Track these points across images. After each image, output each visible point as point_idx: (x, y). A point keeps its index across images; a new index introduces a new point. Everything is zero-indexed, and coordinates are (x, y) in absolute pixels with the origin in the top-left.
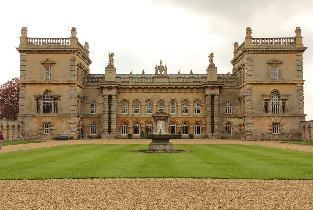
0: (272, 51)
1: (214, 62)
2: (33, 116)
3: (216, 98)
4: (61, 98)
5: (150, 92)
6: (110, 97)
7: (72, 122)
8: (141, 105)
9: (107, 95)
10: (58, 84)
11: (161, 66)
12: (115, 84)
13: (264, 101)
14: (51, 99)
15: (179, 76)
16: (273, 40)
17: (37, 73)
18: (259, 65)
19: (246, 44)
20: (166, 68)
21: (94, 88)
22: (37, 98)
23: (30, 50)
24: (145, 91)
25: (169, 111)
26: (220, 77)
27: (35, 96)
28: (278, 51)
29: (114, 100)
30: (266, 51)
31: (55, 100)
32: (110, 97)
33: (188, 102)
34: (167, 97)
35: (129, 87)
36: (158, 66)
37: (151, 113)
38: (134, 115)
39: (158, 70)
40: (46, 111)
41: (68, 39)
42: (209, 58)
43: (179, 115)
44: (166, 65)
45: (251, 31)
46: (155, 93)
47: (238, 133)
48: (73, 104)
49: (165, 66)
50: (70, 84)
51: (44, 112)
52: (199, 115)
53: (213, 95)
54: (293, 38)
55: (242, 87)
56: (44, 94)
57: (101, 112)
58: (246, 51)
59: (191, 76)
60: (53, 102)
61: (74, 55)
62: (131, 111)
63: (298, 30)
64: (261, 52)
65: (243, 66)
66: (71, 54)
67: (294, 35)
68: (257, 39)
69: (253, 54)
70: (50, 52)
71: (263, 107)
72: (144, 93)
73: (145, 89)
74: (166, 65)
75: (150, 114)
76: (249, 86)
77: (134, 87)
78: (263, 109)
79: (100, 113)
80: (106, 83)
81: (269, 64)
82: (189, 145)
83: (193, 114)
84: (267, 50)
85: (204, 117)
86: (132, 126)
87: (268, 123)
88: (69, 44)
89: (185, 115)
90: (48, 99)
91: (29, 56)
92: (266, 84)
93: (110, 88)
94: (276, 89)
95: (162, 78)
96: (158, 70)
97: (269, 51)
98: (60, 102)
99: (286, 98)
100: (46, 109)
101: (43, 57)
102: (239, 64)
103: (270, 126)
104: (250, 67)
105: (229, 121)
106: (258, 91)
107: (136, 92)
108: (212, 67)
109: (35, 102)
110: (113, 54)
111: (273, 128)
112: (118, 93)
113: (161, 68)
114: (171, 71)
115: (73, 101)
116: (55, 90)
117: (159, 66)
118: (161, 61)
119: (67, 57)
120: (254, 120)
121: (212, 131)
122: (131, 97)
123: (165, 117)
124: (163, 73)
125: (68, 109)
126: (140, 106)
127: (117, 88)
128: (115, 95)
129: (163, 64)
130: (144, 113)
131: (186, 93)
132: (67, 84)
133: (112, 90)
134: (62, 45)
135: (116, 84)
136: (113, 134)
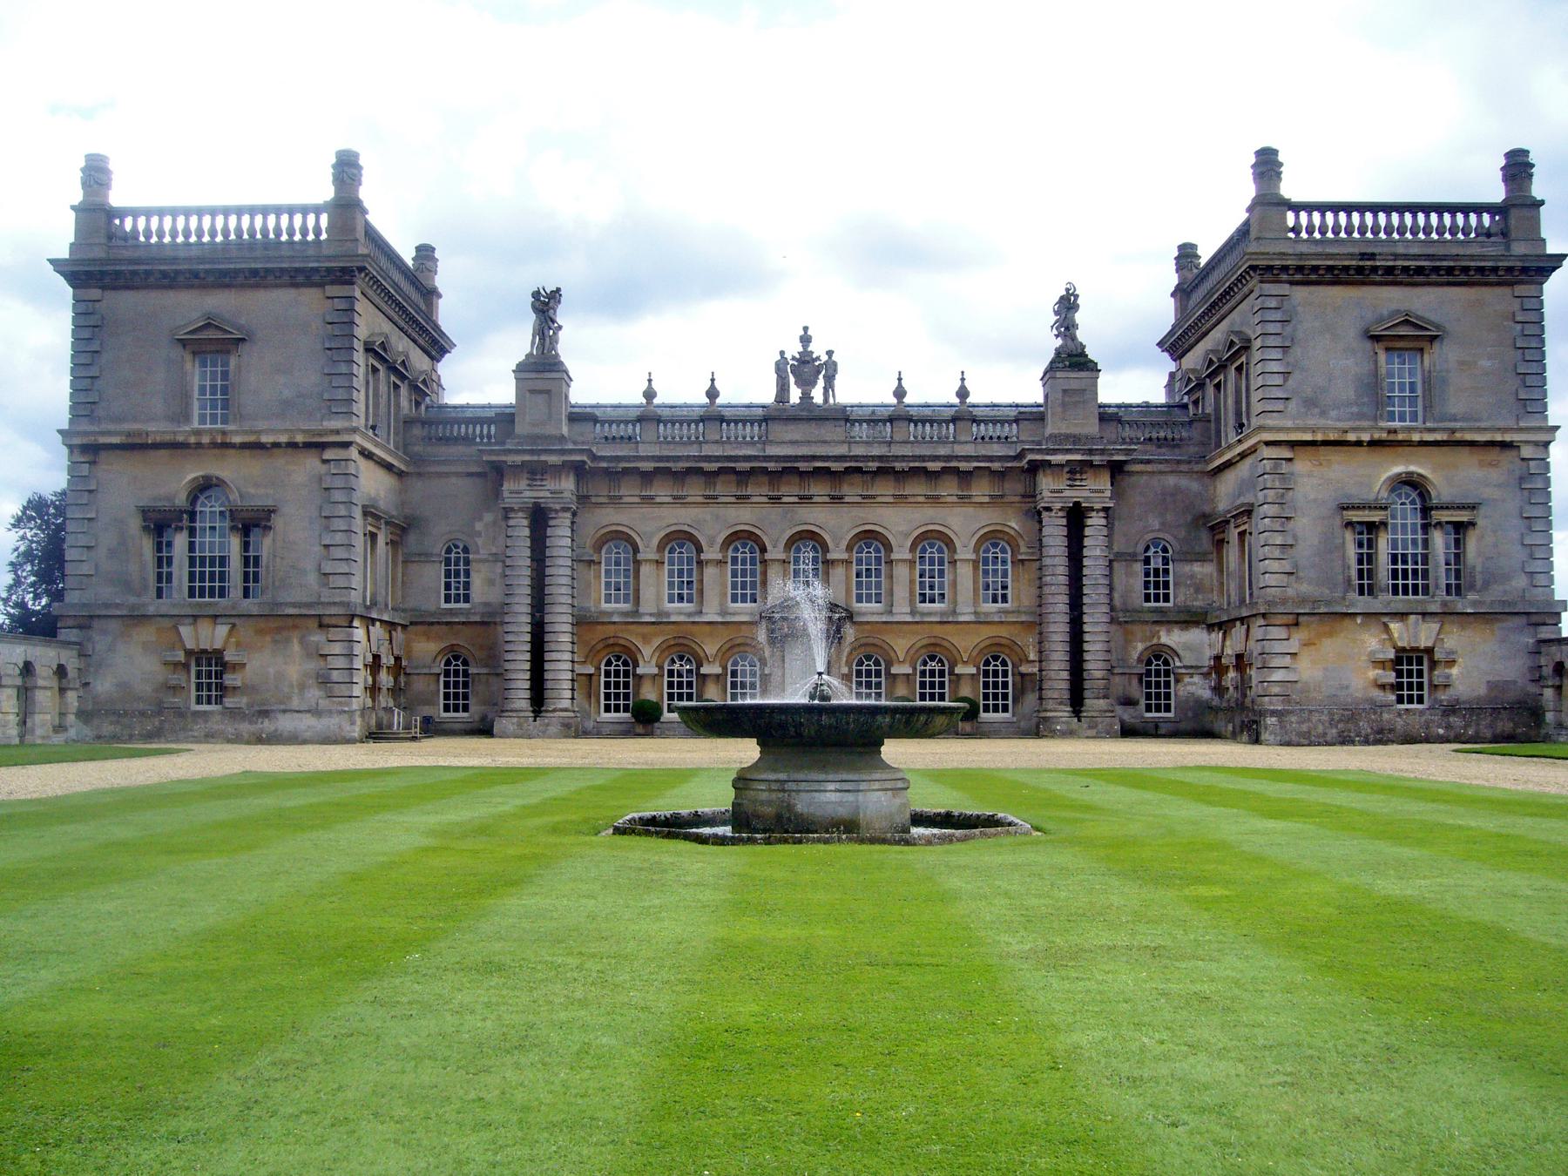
2: (137, 618)
3: (1095, 522)
4: (277, 522)
6: (539, 518)
9: (521, 510)
12: (563, 452)
20: (831, 370)
21: (457, 474)
22: (159, 524)
25: (848, 591)
27: (145, 512)
28: (1420, 271)
29: (560, 536)
32: (539, 518)
33: (950, 543)
36: (788, 356)
38: (668, 614)
39: (792, 379)
41: (317, 210)
42: (1056, 313)
43: (902, 612)
44: (830, 353)
46: (775, 500)
49: (824, 358)
50: (322, 446)
52: (1006, 612)
55: (1229, 465)
63: (1517, 167)
66: (333, 290)
67: (1495, 192)
68: (1309, 208)
69: (1292, 283)
74: (830, 353)
76: (1268, 452)
78: (1349, 580)
81: (1376, 339)
88: (324, 236)
89: (930, 614)
91: (124, 302)
93: (536, 472)
94: (1412, 468)
97: (1374, 269)
103: (1382, 664)
104: (1276, 354)
106: (1319, 483)
109: (147, 545)
110: (556, 295)
112: (583, 499)
113: (806, 367)
114: (859, 388)
116: (245, 479)
118: (806, 329)
120: (1298, 636)
121: (1076, 700)
125: (312, 579)
127: (579, 470)
129: (818, 349)
131: (934, 500)
133: (550, 484)
135: (571, 452)
136: (554, 710)
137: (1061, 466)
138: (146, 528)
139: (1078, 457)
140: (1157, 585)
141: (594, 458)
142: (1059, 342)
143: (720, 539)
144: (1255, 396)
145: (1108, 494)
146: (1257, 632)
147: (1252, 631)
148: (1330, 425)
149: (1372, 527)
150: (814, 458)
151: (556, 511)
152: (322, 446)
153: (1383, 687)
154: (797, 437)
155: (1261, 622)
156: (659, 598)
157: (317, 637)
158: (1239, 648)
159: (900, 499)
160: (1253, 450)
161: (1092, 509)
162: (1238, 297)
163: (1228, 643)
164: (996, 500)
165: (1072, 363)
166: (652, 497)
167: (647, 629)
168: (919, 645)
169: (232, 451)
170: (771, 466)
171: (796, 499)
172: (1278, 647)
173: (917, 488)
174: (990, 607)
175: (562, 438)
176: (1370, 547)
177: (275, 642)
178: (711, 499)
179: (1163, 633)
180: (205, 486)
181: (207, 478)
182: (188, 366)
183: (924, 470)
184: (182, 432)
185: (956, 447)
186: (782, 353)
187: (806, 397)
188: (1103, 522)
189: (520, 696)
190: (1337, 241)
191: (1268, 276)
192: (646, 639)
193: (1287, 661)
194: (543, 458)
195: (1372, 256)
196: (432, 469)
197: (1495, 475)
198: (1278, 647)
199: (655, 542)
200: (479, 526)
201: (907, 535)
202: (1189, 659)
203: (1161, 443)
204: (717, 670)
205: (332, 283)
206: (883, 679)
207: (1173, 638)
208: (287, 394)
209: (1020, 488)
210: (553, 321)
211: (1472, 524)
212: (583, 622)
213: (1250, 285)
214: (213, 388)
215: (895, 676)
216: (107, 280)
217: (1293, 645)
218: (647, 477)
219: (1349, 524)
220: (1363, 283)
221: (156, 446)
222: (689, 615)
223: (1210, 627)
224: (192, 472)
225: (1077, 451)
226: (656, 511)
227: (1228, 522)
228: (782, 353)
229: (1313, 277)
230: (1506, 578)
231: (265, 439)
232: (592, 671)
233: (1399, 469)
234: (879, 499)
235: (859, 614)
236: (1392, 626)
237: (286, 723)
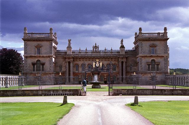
2: (31, 74)
3: (124, 63)
4: (45, 64)
6: (69, 63)
7: (52, 76)
10: (43, 57)
13: (147, 65)
15: (105, 51)
17: (33, 52)
18: (146, 46)
26: (127, 52)
27: (32, 63)
28: (155, 40)
29: (71, 65)
31: (42, 65)
32: (69, 63)
47: (168, 73)
48: (51, 67)
51: (37, 71)
52: (116, 72)
54: (163, 33)
55: (137, 58)
56: (37, 62)
57: (65, 70)
59: (112, 51)
60: (41, 66)
61: (51, 42)
62: (80, 70)
66: (50, 42)
70: (154, 40)
76: (140, 57)
81: (150, 46)
82: (45, 102)
85: (118, 73)
91: (29, 43)
92: (148, 56)
93: (69, 58)
99: (159, 63)
101: (36, 43)
106: (144, 60)
108: (122, 47)
109: (32, 66)
112: (73, 60)
113: (96, 47)
114: (101, 48)
115: (51, 66)
116: (157, 60)
120: (142, 75)
121: (122, 80)
122: (80, 63)
125: (49, 70)
129: (97, 45)
131: (109, 61)
138: (32, 65)
148: (146, 55)
153: (150, 79)
157: (50, 75)
159: (105, 61)
170: (92, 57)
180: (38, 60)
184: (36, 55)
187: (96, 50)
189: (67, 81)
190: (146, 37)
195: (150, 38)
197: (162, 59)
199: (81, 65)
203: (132, 55)
208: (46, 52)
209: (117, 59)
211: (159, 64)
212: (74, 73)
217: (142, 75)
218: (80, 58)
219: (147, 64)
221: (33, 57)
226: (81, 62)
230: (163, 69)
231: (44, 56)
237: (47, 83)
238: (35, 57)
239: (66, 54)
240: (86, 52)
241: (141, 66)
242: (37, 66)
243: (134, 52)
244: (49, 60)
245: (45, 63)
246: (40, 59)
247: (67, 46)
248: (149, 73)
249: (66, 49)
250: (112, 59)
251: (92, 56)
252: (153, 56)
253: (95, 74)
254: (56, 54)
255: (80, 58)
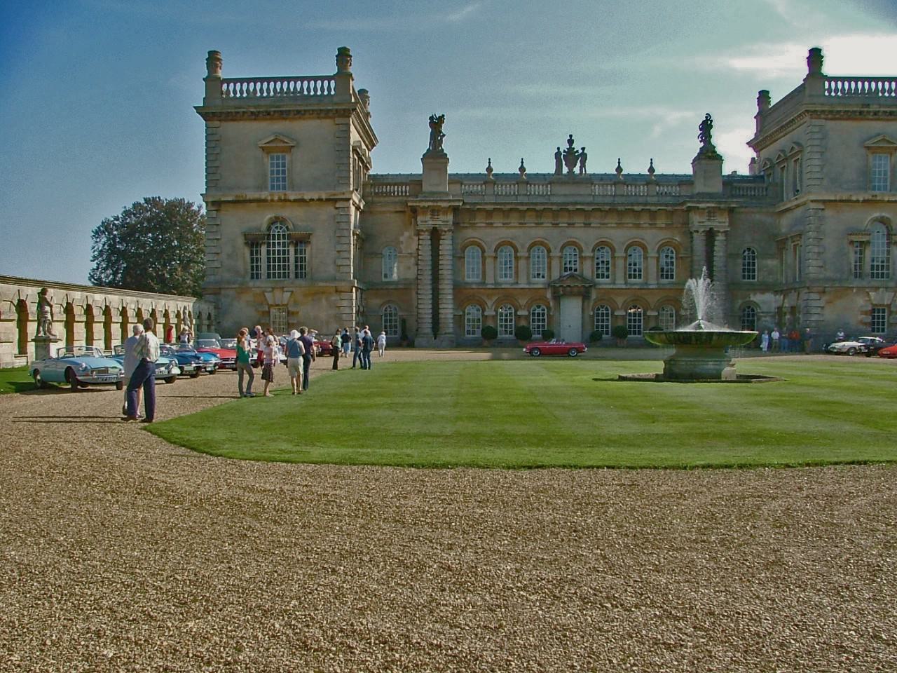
0: (876, 113)
1: (713, 141)
3: (720, 237)
4: (313, 240)
5: (606, 221)
6: (435, 234)
8: (581, 257)
9: (427, 231)
11: (571, 151)
12: (450, 201)
14: (286, 241)
15: (619, 179)
16: (252, 84)
19: (807, 92)
20: (584, 156)
21: (391, 212)
22: (253, 242)
23: (231, 112)
24: (530, 220)
25: (593, 272)
29: (446, 245)
30: (861, 113)
31: (296, 245)
32: (435, 234)
33: (644, 248)
34: (586, 236)
35: (535, 209)
36: (562, 150)
37: (543, 277)
38: (501, 284)
39: (564, 163)
40: (274, 274)
41: (329, 78)
42: (701, 129)
43: (620, 283)
44: (583, 149)
45: (823, 57)
46: (556, 225)
49: (580, 151)
50: (336, 200)
51: (269, 276)
52: (673, 283)
53: (711, 229)
55: (789, 210)
56: (269, 229)
57: (411, 274)
58: (807, 111)
59: (651, 179)
60: (292, 249)
64: (849, 116)
65: (794, 154)
66: (338, 120)
68: (836, 79)
69: (826, 119)
70: (283, 115)
71: (850, 264)
72: (525, 224)
73: (530, 213)
74: (583, 149)
75: (539, 283)
76: (813, 206)
77: (499, 207)
78: (851, 270)
79: (406, 279)
80: (425, 197)
81: (868, 148)
83: (656, 282)
84: (862, 109)
86: (494, 313)
87: (862, 307)
88: (333, 93)
89: (634, 284)
90: (279, 243)
91: (231, 129)
92: (858, 201)
93: (435, 211)
94: (884, 214)
95: (574, 183)
96: (564, 163)
97: (869, 112)
98: (311, 249)
99: (864, 239)
100: (274, 269)
101: (262, 130)
102: (784, 142)
103: (866, 313)
104: (817, 156)
105: (752, 299)
106: (835, 222)
107: (536, 222)
109: (247, 251)
110: (441, 119)
111: (873, 318)
112: (456, 224)
113: (571, 156)
114: (598, 165)
116: (296, 217)
117: (564, 151)
118: (571, 136)
119: (324, 127)
120: (825, 298)
122: (490, 234)
123: (582, 290)
124: (577, 170)
126: (578, 259)
127: (455, 210)
128: (449, 231)
129: (577, 147)
130: (533, 277)
131: (637, 226)
132: (328, 200)
133: (442, 217)
134: (232, 98)
135: (453, 201)
136: (446, 334)
137: (704, 209)
139: (713, 205)
140: (749, 270)
141: (464, 204)
142: (702, 144)
143: (527, 245)
144: (806, 177)
145: (727, 224)
146: (804, 296)
147: (801, 296)
149: (863, 244)
150: (576, 204)
151: (445, 232)
152: (336, 200)
153: (866, 324)
154: (567, 193)
155: (806, 291)
156: (495, 276)
157: (334, 297)
158: (793, 303)
160: (804, 204)
161: (719, 232)
162: (797, 125)
163: (786, 301)
164: (669, 226)
165: (709, 156)
166: (492, 224)
167: (490, 291)
168: (628, 300)
169: (288, 203)
170: (554, 208)
171: (566, 225)
172: (814, 304)
173: (629, 220)
174: (665, 281)
175: (447, 194)
176: (861, 254)
177: (313, 300)
178: (522, 225)
179: (751, 296)
181: (277, 218)
182: (266, 160)
183: (633, 211)
185: (648, 198)
186: (558, 148)
188: (724, 238)
190: (262, 97)
191: (814, 116)
192: (489, 296)
193: (819, 311)
194: (439, 204)
196: (379, 209)
198: (814, 304)
200: (401, 239)
201: (623, 244)
202: (765, 309)
204: (526, 313)
205: (339, 117)
206: (610, 318)
207: (757, 298)
210: (441, 132)
213: (805, 120)
214: (278, 171)
215: (649, 316)
216: (223, 116)
218: (489, 214)
220: (862, 119)
222: (512, 284)
223: (776, 293)
224: (269, 215)
225: (713, 202)
227: (787, 239)
228: (558, 148)
229: (837, 116)
232: (461, 313)
233: (877, 215)
234: (609, 225)
235: (600, 284)
236: (870, 293)
238: (259, 201)
239: (421, 191)
240: (522, 179)
241: (819, 253)
242: (268, 253)
243: (762, 186)
244: (334, 217)
245: (310, 234)
246: (285, 213)
247: (425, 146)
248: (861, 289)
249: (690, 171)
250: (653, 215)
251: (554, 200)
252: (882, 201)
253: (571, 294)
254: (368, 190)
255: (489, 214)
